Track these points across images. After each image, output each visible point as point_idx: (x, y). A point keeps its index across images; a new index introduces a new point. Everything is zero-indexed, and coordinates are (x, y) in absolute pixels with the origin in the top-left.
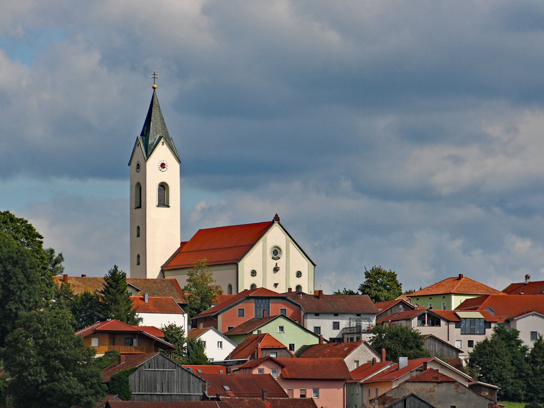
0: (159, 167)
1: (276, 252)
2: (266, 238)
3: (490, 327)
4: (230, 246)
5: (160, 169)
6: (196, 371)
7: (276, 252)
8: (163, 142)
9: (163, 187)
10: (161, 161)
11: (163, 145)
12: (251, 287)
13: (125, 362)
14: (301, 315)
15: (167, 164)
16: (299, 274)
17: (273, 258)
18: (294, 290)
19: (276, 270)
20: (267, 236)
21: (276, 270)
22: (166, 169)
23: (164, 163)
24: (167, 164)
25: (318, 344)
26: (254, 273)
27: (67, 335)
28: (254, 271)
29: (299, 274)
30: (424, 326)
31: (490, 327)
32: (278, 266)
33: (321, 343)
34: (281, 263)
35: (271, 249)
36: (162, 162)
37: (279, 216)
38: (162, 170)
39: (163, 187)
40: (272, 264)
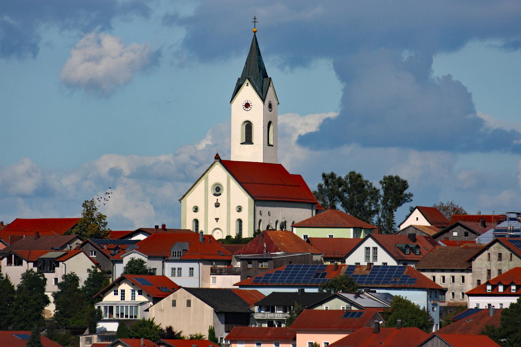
1: (218, 190)
3: (34, 266)
5: (244, 109)
7: (218, 190)
8: (247, 83)
9: (248, 126)
10: (245, 101)
11: (247, 85)
12: (198, 221)
13: (370, 290)
14: (513, 236)
15: (251, 103)
16: (240, 209)
19: (217, 205)
22: (250, 108)
23: (248, 102)
24: (251, 103)
26: (196, 209)
27: (93, 274)
28: (195, 207)
29: (240, 209)
30: (11, 266)
31: (34, 266)
32: (219, 202)
34: (222, 199)
35: (212, 186)
37: (219, 156)
38: (246, 110)
39: (248, 126)
40: (213, 199)
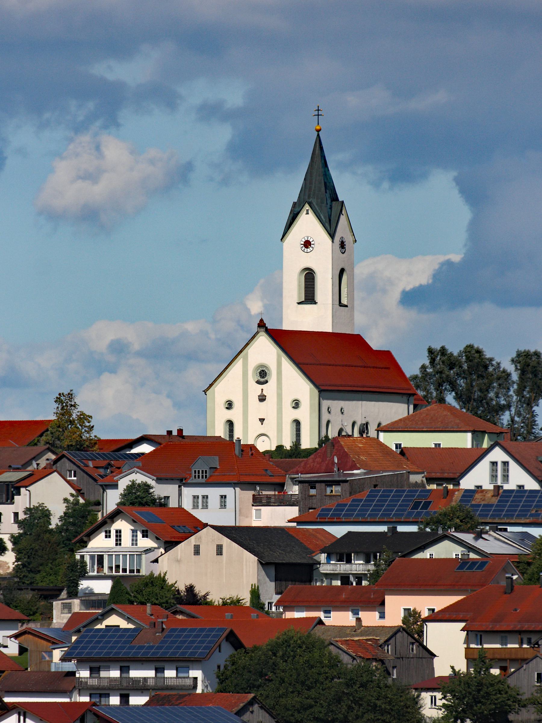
0: (302, 247)
2: (247, 353)
4: (382, 366)
6: (314, 507)
10: (304, 238)
16: (296, 405)
17: (258, 382)
18: (175, 433)
19: (262, 398)
20: (249, 351)
21: (262, 398)
22: (311, 249)
23: (309, 239)
24: (313, 241)
25: (176, 508)
26: (230, 405)
29: (296, 405)
33: (479, 447)
34: (270, 389)
36: (306, 239)
37: (265, 322)
38: (306, 251)
40: (255, 390)
